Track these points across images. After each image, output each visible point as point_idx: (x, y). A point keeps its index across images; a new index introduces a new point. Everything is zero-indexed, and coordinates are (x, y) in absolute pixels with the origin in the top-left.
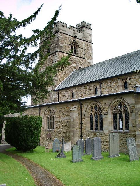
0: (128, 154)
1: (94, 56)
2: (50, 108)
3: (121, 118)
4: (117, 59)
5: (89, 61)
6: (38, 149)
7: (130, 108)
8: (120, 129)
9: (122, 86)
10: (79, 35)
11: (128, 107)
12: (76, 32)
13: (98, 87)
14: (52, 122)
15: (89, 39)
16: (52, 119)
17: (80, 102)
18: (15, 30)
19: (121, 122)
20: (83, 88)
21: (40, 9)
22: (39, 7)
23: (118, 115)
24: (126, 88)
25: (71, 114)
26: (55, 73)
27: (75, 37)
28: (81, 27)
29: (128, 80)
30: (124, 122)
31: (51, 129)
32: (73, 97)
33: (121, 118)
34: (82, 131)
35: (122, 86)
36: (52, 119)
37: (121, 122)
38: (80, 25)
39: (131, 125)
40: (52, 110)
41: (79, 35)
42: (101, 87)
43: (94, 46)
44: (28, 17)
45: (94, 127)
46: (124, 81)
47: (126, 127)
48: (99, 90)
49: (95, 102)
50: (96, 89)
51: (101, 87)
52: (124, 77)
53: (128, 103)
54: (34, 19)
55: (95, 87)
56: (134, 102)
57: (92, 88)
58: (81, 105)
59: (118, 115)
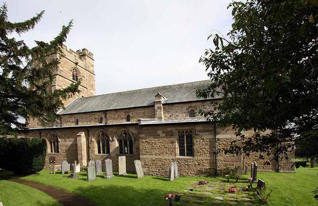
0: (136, 174)
1: (96, 87)
2: (53, 132)
3: (126, 144)
4: (120, 94)
5: (92, 91)
6: (41, 172)
7: (134, 137)
8: (126, 153)
9: (125, 118)
10: (80, 62)
11: (132, 136)
12: (77, 58)
13: (103, 117)
14: (56, 145)
15: (91, 69)
16: (56, 143)
17: (87, 129)
18: (66, 26)
19: (126, 148)
20: (88, 116)
21: (40, 16)
22: (39, 13)
23: (123, 142)
24: (128, 120)
25: (78, 138)
26: (65, 97)
27: (76, 64)
28: (82, 54)
29: (131, 114)
30: (129, 148)
31: (187, 156)
32: (77, 124)
33: (126, 144)
34: (90, 154)
35: (125, 118)
36: (56, 143)
37: (126, 148)
38: (81, 51)
39: (134, 150)
40: (55, 134)
41: (80, 62)
42: (106, 117)
43: (96, 77)
44: (22, 21)
45: (53, 151)
46: (127, 114)
47: (130, 151)
48: (104, 119)
49: (101, 130)
50: (101, 118)
51: (106, 117)
52: (127, 110)
53: (132, 133)
54: (32, 27)
55: (100, 117)
56: (137, 133)
57: (97, 117)
58: (88, 131)
59: (123, 142)
